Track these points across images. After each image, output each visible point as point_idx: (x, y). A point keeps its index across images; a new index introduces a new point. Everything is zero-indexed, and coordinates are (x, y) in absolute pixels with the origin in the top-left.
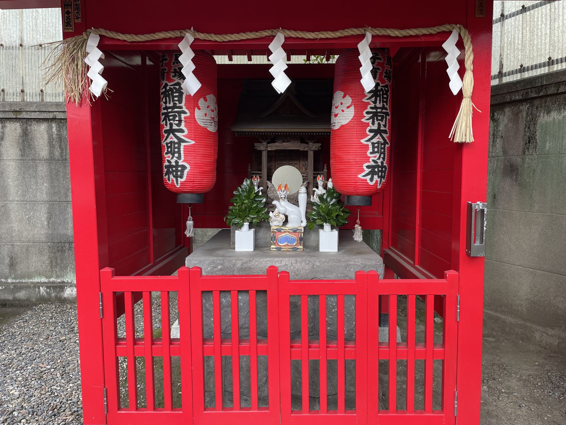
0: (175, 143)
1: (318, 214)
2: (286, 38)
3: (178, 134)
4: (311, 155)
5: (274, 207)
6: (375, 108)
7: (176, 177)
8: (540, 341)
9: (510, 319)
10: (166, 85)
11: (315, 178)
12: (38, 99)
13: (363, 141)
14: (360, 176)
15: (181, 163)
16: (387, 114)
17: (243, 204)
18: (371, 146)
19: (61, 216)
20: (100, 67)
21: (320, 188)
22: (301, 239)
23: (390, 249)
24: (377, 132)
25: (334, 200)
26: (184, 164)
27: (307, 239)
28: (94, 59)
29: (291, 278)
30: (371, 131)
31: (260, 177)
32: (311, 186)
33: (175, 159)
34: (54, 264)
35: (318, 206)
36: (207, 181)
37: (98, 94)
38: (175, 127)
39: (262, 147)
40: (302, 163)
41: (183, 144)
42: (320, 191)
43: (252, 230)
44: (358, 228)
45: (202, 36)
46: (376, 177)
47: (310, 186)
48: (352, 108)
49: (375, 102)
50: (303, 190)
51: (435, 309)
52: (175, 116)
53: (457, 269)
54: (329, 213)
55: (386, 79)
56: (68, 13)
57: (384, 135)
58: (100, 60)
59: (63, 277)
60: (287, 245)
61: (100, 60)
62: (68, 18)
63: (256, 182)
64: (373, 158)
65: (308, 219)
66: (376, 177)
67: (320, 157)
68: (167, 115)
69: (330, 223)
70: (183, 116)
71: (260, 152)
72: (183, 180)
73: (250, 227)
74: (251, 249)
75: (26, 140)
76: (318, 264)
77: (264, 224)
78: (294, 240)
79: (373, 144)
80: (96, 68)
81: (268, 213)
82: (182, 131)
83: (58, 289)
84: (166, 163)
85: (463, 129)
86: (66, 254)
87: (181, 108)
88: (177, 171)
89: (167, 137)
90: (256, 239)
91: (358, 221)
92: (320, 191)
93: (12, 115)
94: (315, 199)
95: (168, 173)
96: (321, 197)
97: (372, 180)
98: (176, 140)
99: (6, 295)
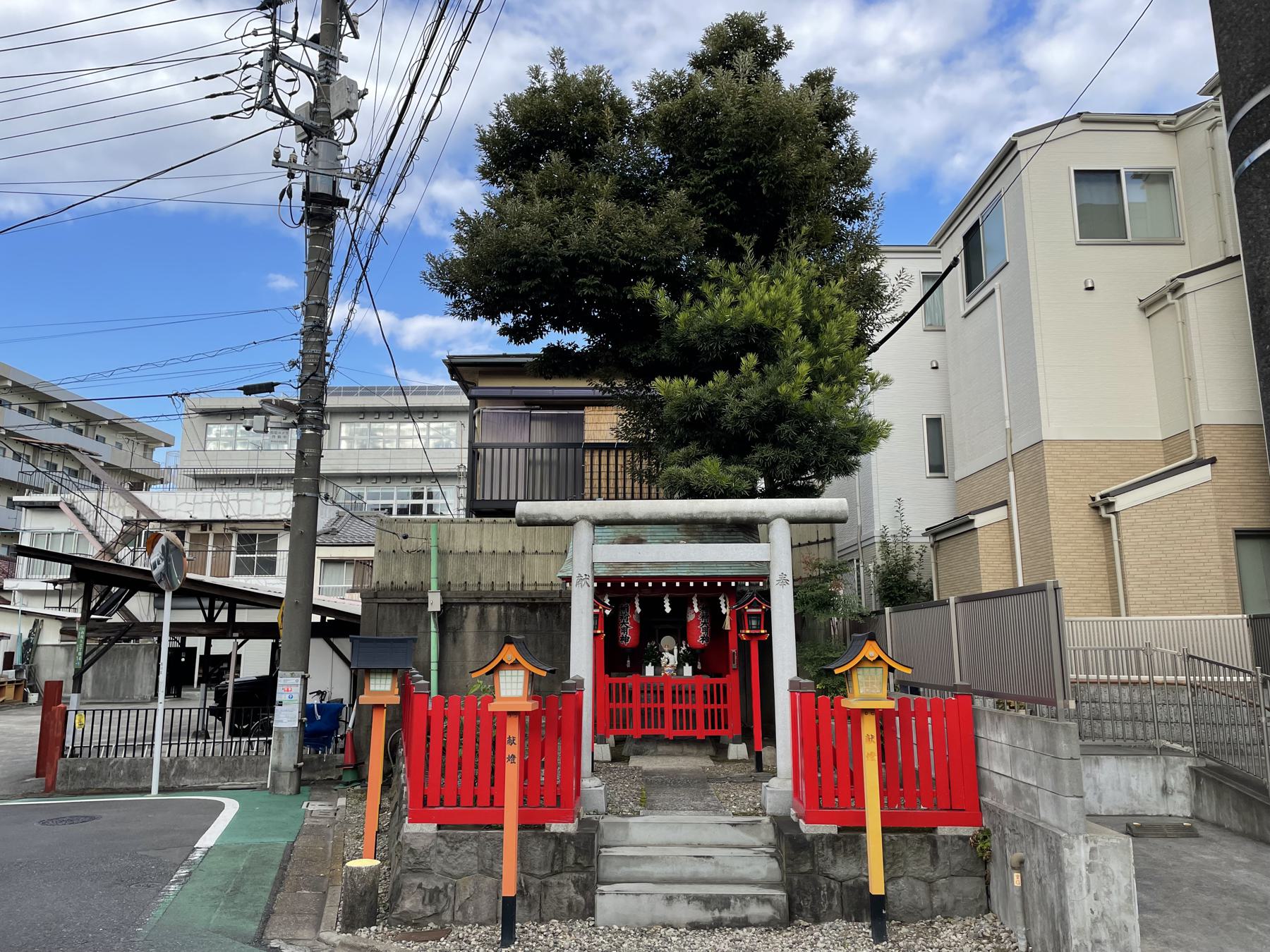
36: (636, 643)
51: (818, 497)
67: (681, 633)
75: (482, 618)
85: (727, 626)
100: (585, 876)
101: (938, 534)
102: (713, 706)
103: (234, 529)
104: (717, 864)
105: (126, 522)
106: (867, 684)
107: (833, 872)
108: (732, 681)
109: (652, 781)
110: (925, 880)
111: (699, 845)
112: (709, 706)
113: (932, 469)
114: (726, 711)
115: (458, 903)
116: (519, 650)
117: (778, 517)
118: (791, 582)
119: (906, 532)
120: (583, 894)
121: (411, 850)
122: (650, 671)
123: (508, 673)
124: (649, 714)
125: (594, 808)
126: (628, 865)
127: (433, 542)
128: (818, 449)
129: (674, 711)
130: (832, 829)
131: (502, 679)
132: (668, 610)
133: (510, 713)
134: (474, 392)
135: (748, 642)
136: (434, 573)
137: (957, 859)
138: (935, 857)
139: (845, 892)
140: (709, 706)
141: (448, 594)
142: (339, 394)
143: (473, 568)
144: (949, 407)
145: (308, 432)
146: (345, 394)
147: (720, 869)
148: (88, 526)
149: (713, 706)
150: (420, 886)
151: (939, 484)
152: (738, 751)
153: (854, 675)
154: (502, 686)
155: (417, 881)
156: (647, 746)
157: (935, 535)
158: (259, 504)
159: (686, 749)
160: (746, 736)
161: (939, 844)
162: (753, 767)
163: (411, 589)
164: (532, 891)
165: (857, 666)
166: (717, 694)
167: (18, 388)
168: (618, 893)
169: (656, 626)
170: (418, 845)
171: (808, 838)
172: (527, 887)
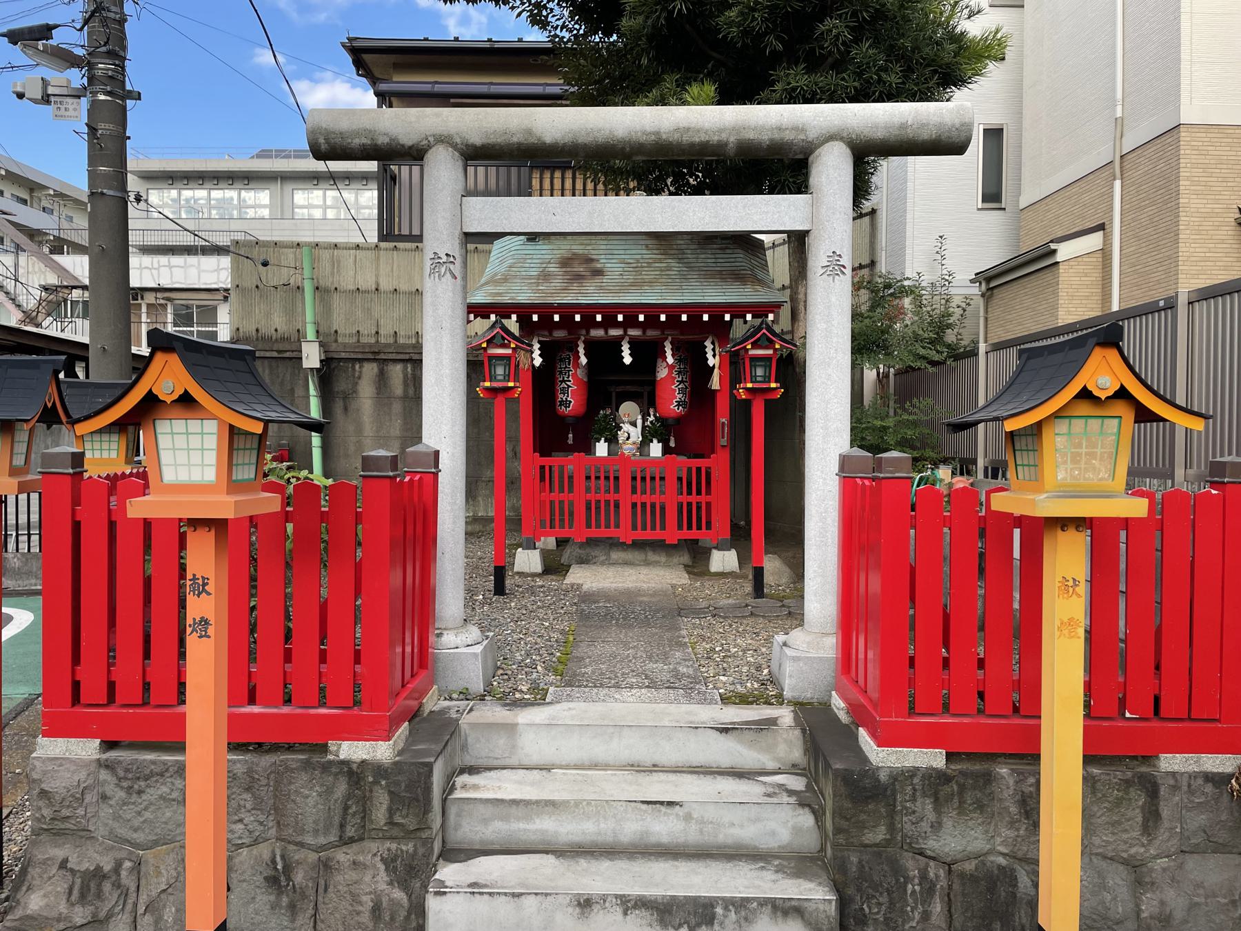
4: (646, 394)
12: (391, 341)
44: (672, 439)
54: (656, 431)
67: (647, 397)
75: (382, 380)
80: (537, 353)
85: (715, 383)
93: (371, 356)
100: (408, 847)
101: (993, 281)
102: (690, 498)
103: (168, 299)
104: (688, 817)
105: (45, 288)
106: (1076, 459)
107: (932, 845)
108: (719, 464)
109: (597, 613)
110: (1125, 862)
111: (655, 768)
112: (685, 499)
113: (985, 199)
114: (708, 505)
115: (143, 899)
116: (191, 367)
117: (831, 138)
118: (848, 271)
119: (947, 281)
120: (404, 885)
121: (44, 794)
122: (602, 449)
123: (179, 425)
124: (598, 508)
125: (461, 685)
126: (505, 818)
127: (307, 273)
128: (885, 70)
129: (634, 505)
130: (934, 758)
131: (164, 441)
132: (628, 360)
133: (195, 523)
134: (383, 87)
135: (747, 404)
136: (309, 317)
137: (1199, 820)
138: (1152, 817)
139: (956, 886)
140: (685, 499)
141: (333, 347)
142: (290, 157)
143: (369, 311)
144: (1019, 114)
145: (102, 97)
146: (296, 157)
147: (694, 827)
148: (7, 293)
149: (690, 498)
150: (63, 864)
151: (993, 218)
152: (724, 560)
153: (1047, 434)
154: (166, 457)
155: (59, 853)
156: (595, 552)
157: (989, 280)
158: (193, 272)
159: (652, 556)
160: (739, 537)
161: (1163, 791)
162: (749, 588)
163: (283, 339)
164: (299, 877)
165: (1057, 415)
166: (698, 482)
167: (12, 177)
168: (475, 888)
169: (613, 383)
170: (59, 783)
171: (883, 776)
172: (288, 869)
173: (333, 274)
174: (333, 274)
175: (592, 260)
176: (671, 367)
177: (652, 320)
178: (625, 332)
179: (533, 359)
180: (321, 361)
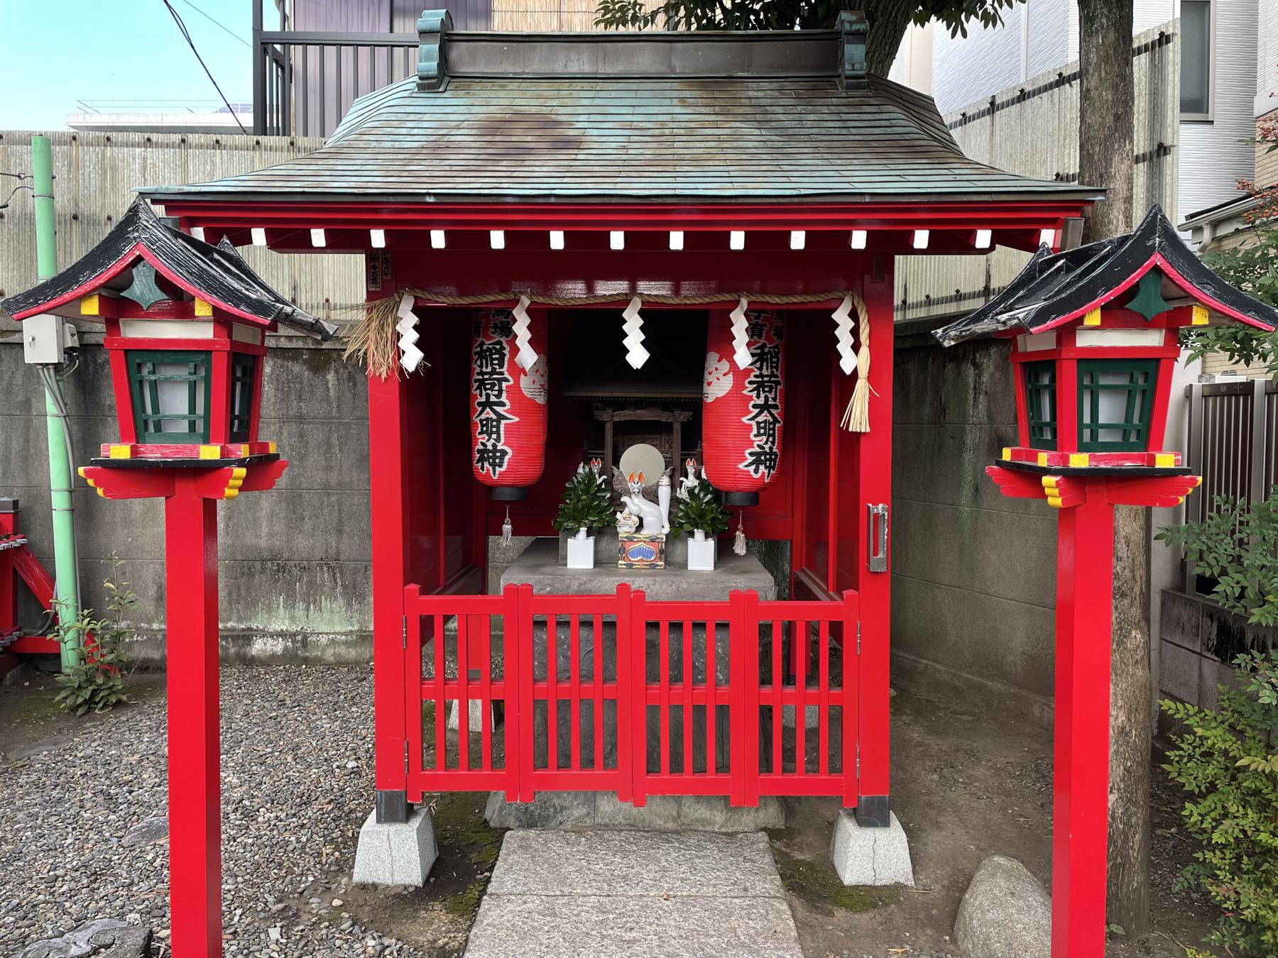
0: (492, 420)
1: (687, 516)
2: (643, 303)
3: (497, 409)
4: (677, 428)
5: (624, 505)
6: (761, 376)
7: (494, 465)
8: (1041, 719)
9: (998, 687)
10: (483, 343)
11: (683, 461)
13: (744, 420)
14: (741, 466)
15: (500, 447)
16: (777, 383)
17: (579, 500)
18: (755, 427)
19: (249, 515)
20: (416, 336)
21: (691, 477)
22: (662, 552)
23: (803, 571)
24: (763, 408)
25: (709, 496)
26: (505, 448)
27: (670, 551)
28: (407, 324)
29: (648, 599)
30: (755, 406)
31: (602, 460)
32: (677, 474)
33: (492, 441)
34: (235, 596)
35: (686, 504)
36: (532, 471)
37: (411, 368)
38: (493, 399)
39: (606, 416)
40: (665, 437)
41: (503, 422)
42: (691, 482)
43: (592, 539)
44: (740, 536)
45: (541, 299)
46: (762, 468)
47: (676, 474)
48: (731, 375)
49: (760, 369)
50: (665, 481)
52: (493, 385)
53: (856, 589)
54: (702, 515)
55: (775, 338)
56: (375, 267)
57: (774, 412)
58: (416, 328)
59: (249, 619)
60: (641, 560)
61: (416, 328)
62: (374, 274)
63: (596, 467)
64: (758, 442)
65: (671, 522)
66: (762, 468)
67: (685, 432)
68: (482, 384)
69: (703, 528)
70: (504, 384)
71: (604, 423)
72: (504, 469)
73: (588, 535)
74: (591, 566)
76: (685, 586)
77: (609, 530)
78: (651, 553)
79: (758, 423)
80: (409, 337)
81: (615, 513)
82: (503, 404)
83: (241, 641)
84: (480, 447)
85: (858, 416)
86: (256, 581)
87: (502, 373)
88: (494, 457)
89: (482, 412)
90: (596, 552)
91: (740, 526)
92: (691, 482)
94: (683, 494)
95: (481, 460)
96: (691, 492)
97: (756, 471)
98: (494, 417)
99: (149, 652)
132: (637, 357)
173: (103, 191)
174: (103, 191)
175: (557, 124)
176: (740, 375)
177: (707, 244)
178: (633, 289)
179: (399, 353)
180: (68, 351)
